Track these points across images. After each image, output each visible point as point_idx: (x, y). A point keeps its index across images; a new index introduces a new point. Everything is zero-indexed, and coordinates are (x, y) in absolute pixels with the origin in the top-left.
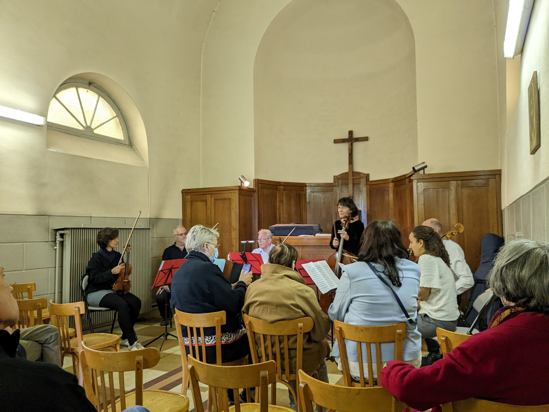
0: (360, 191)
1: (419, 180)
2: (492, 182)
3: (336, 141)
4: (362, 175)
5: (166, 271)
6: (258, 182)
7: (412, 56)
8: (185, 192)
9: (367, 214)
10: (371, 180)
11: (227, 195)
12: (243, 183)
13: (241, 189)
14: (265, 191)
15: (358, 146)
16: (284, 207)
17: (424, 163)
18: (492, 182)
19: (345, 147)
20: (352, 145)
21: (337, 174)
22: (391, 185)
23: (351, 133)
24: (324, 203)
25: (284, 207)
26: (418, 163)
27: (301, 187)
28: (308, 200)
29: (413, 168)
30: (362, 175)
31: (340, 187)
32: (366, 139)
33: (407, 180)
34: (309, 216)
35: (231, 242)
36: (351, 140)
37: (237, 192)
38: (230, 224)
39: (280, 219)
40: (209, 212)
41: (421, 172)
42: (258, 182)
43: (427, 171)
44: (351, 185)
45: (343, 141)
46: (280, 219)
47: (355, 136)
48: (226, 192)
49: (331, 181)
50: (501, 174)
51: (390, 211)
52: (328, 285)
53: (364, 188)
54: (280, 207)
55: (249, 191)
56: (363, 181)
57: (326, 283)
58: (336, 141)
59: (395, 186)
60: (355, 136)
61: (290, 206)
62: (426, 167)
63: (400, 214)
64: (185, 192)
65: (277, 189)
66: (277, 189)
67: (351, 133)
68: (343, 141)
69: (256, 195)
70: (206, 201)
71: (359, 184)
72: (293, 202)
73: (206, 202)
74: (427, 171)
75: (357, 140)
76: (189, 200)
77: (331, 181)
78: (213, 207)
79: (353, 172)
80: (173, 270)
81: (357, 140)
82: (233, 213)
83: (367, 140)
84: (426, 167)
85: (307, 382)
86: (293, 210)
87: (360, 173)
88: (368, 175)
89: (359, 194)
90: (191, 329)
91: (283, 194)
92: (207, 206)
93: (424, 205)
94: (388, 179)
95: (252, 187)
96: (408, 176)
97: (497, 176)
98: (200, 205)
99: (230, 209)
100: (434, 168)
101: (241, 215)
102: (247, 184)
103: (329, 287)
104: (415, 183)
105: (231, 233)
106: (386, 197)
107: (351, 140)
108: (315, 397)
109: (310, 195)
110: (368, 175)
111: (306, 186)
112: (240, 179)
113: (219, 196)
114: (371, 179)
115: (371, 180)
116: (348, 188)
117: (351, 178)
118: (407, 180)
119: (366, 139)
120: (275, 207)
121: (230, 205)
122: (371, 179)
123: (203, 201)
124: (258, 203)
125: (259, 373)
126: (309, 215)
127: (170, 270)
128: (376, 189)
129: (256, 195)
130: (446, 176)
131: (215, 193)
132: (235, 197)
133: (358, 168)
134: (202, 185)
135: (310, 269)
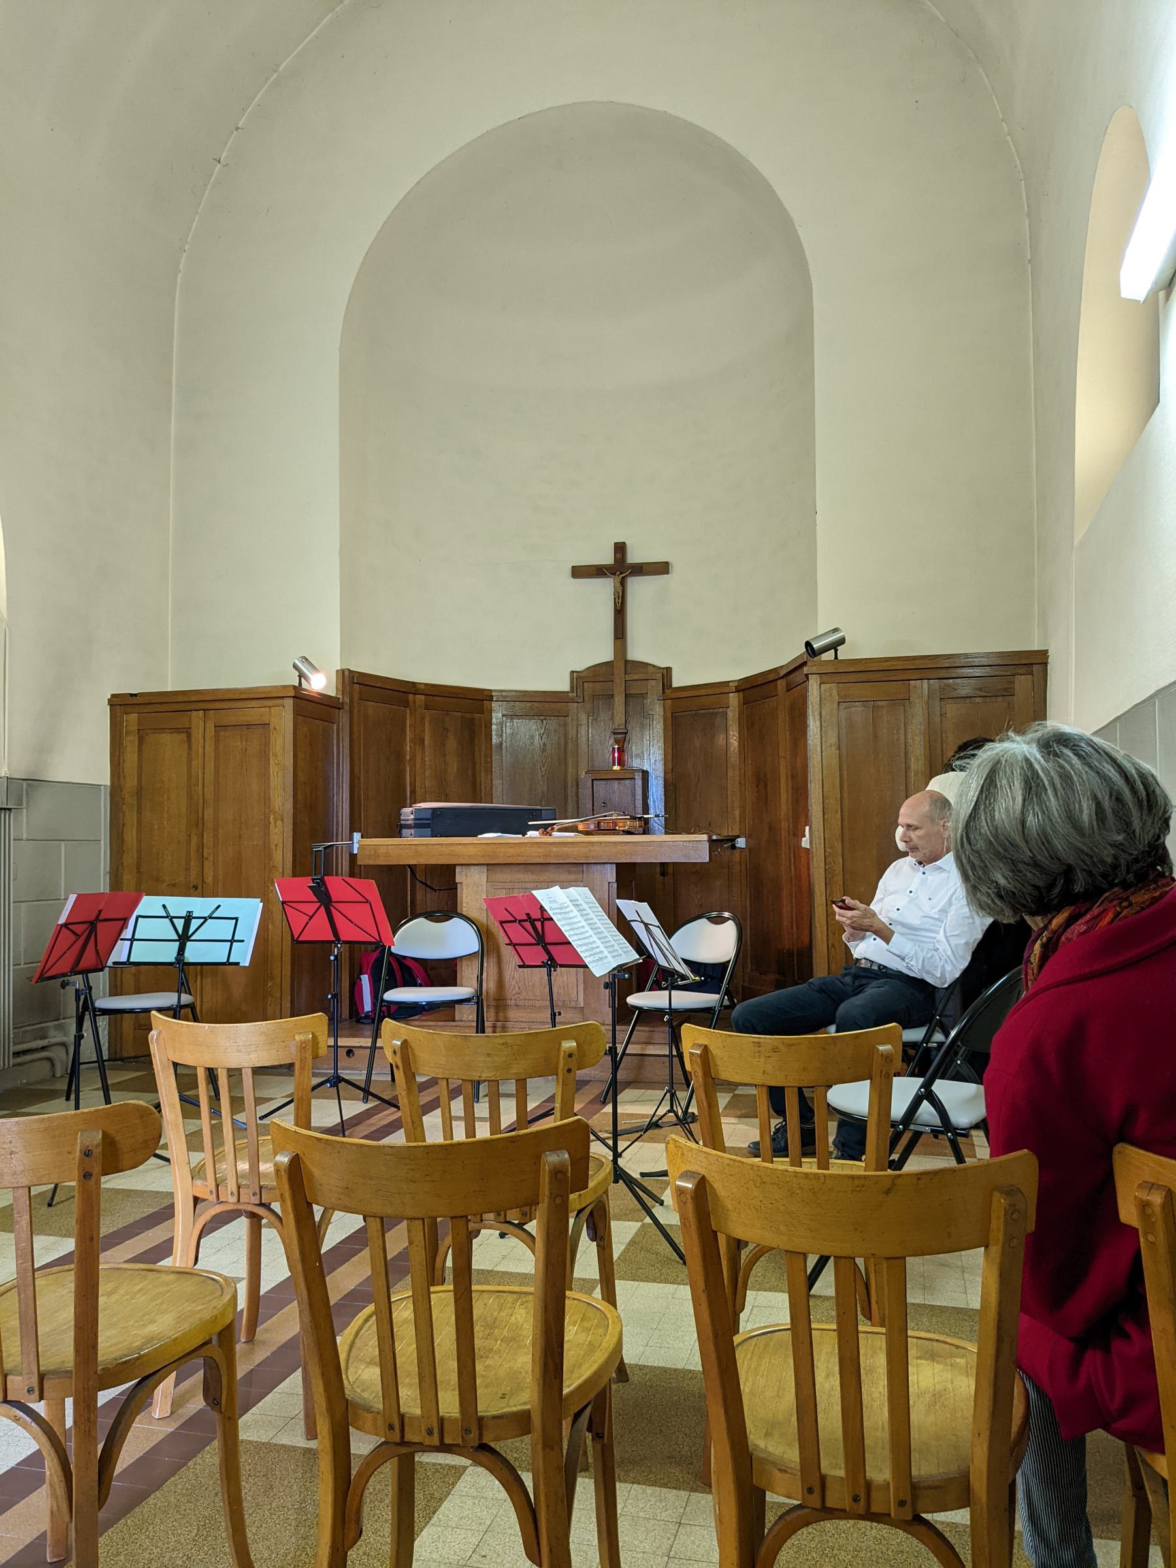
0: (646, 715)
1: (825, 678)
2: (1022, 683)
3: (579, 572)
4: (651, 669)
5: (78, 929)
6: (352, 680)
7: (800, 336)
8: (120, 704)
9: (665, 781)
10: (674, 685)
11: (254, 713)
12: (307, 679)
13: (301, 699)
14: (371, 708)
15: (638, 587)
16: (424, 756)
17: (836, 630)
18: (1022, 683)
19: (604, 589)
20: (623, 583)
21: (580, 666)
22: (734, 699)
23: (620, 548)
24: (544, 751)
25: (424, 756)
26: (820, 630)
27: (473, 703)
28: (495, 740)
29: (808, 644)
30: (651, 669)
31: (588, 705)
32: (663, 568)
33: (781, 684)
34: (498, 786)
35: (269, 856)
36: (621, 568)
37: (289, 703)
38: (266, 800)
39: (413, 792)
40: (196, 763)
41: (829, 656)
42: (352, 680)
43: (844, 653)
44: (619, 700)
45: (598, 571)
46: (413, 792)
47: (633, 557)
48: (254, 703)
49: (564, 685)
50: (1046, 664)
51: (730, 773)
52: (606, 953)
53: (658, 710)
54: (413, 759)
55: (324, 704)
56: (655, 687)
57: (602, 948)
58: (579, 572)
59: (745, 702)
60: (633, 557)
61: (444, 755)
62: (842, 641)
63: (758, 780)
64: (120, 704)
65: (406, 704)
66: (406, 704)
67: (620, 548)
68: (598, 571)
69: (344, 718)
70: (188, 732)
71: (643, 696)
72: (452, 743)
73: (189, 736)
74: (844, 653)
75: (640, 570)
76: (134, 728)
77: (564, 685)
78: (210, 749)
79: (626, 662)
80: (100, 926)
81: (640, 570)
82: (273, 769)
83: (667, 572)
84: (842, 641)
85: (703, 1172)
86: (453, 768)
87: (647, 664)
88: (669, 670)
89: (642, 726)
90: (212, 1074)
91: (423, 718)
92: (190, 747)
93: (839, 748)
94: (726, 684)
95: (332, 693)
96: (782, 673)
97: (1035, 668)
98: (169, 745)
99: (264, 755)
100: (866, 643)
101: (300, 774)
102: (320, 683)
103: (610, 959)
104: (813, 685)
105: (267, 826)
106: (721, 740)
107: (621, 568)
108: (733, 1216)
109: (501, 724)
110: (669, 670)
111: (491, 698)
112: (295, 667)
113: (231, 718)
114: (676, 683)
115: (674, 685)
116: (611, 707)
117: (617, 684)
118: (781, 684)
119: (663, 568)
120: (398, 756)
121: (267, 744)
122: (676, 683)
123: (178, 730)
124: (351, 740)
125: (538, 1158)
126: (497, 782)
127: (92, 925)
128: (691, 711)
129: (344, 718)
130: (900, 665)
131: (210, 706)
132: (283, 719)
133: (637, 653)
134: (171, 679)
135: (554, 905)
